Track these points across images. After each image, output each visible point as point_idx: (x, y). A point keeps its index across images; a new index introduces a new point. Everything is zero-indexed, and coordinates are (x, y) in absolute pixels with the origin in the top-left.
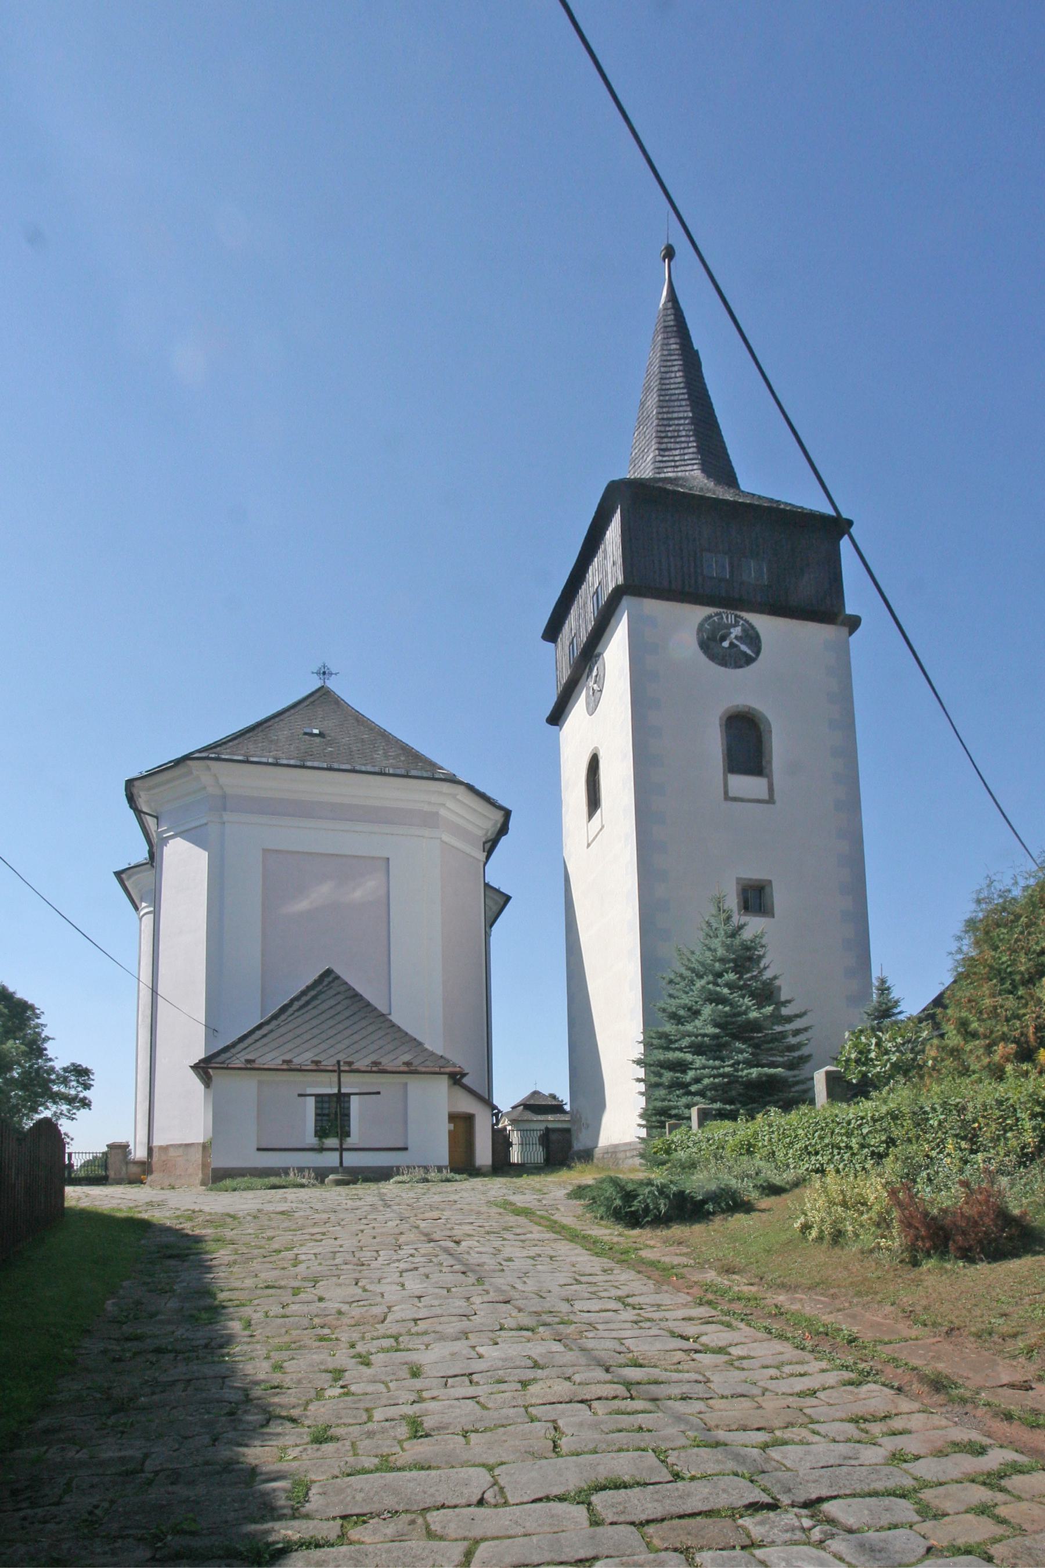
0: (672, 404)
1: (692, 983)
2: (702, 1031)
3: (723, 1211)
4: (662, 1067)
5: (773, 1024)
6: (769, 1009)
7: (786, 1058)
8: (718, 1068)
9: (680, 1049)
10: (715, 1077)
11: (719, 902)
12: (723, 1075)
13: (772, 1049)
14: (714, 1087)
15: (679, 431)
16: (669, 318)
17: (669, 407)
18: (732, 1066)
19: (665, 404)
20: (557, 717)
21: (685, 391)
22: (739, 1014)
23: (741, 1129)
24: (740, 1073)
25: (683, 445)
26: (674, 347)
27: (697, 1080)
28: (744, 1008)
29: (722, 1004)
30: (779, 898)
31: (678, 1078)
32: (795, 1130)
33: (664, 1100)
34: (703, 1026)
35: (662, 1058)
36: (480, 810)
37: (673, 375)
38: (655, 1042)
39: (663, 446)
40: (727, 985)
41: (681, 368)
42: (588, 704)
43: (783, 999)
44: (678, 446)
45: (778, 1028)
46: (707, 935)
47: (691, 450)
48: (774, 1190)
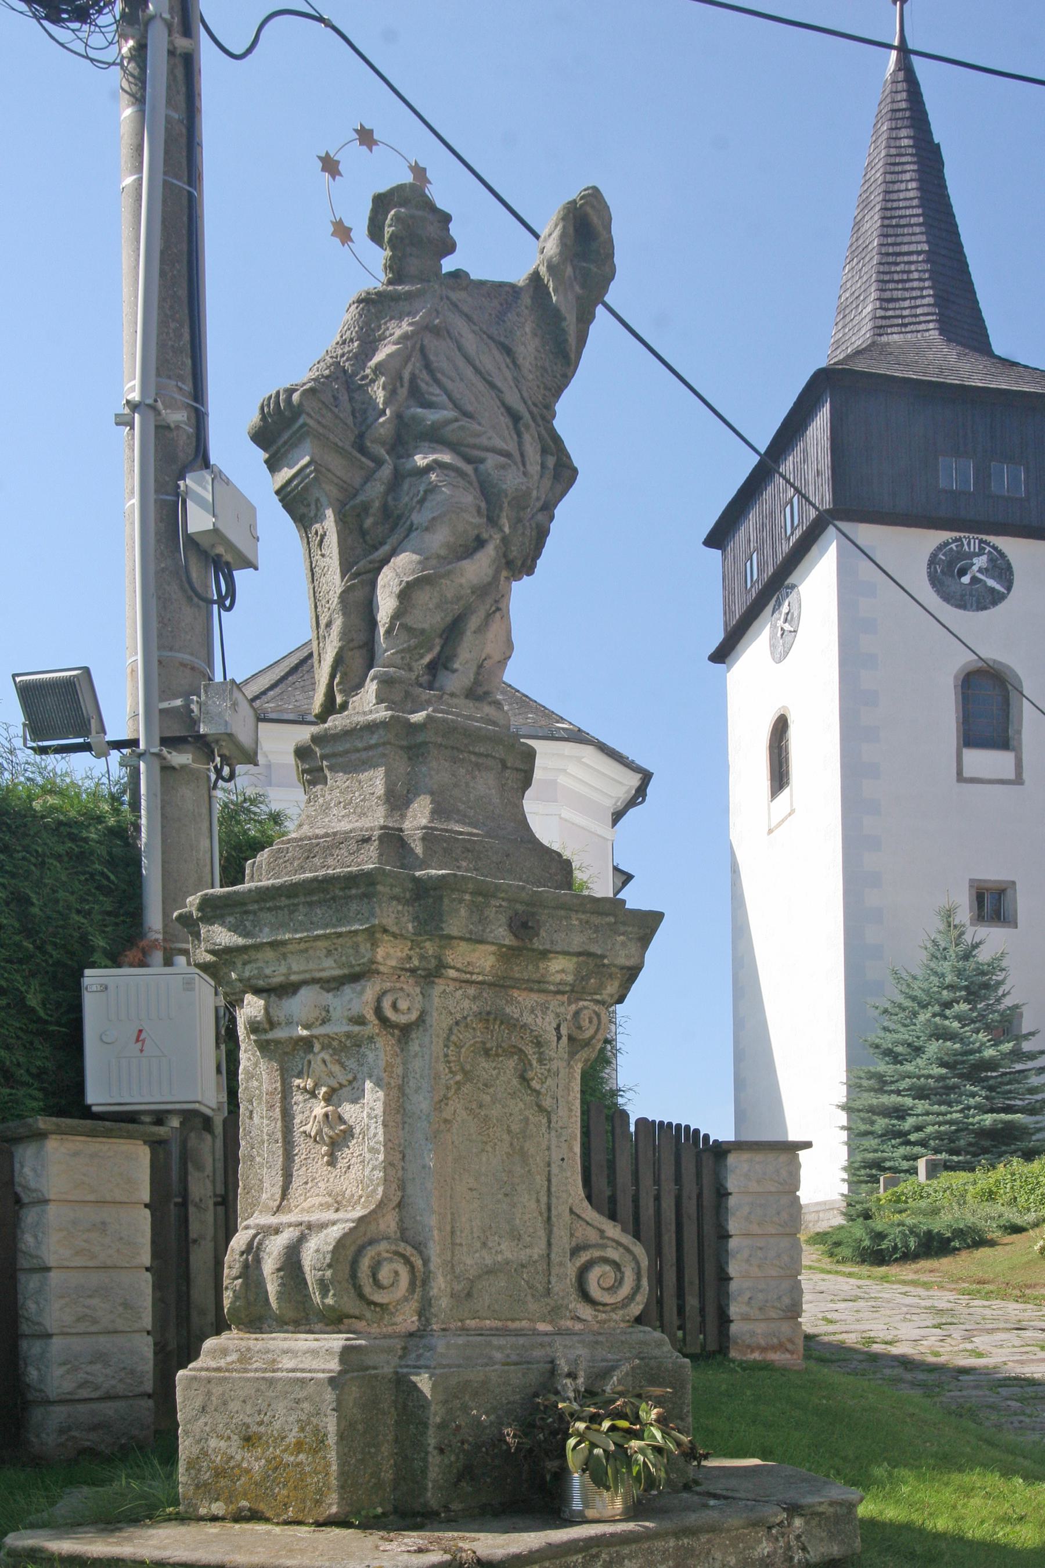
0: (900, 231)
1: (915, 1014)
2: (925, 1072)
3: (969, 1247)
4: (874, 1113)
5: (1012, 1062)
6: (1007, 1047)
7: (1027, 1102)
8: (944, 1114)
9: (898, 1093)
10: (940, 1124)
11: (948, 914)
12: (950, 1123)
13: (1010, 1092)
14: (939, 1136)
15: (909, 272)
16: (899, 97)
17: (897, 235)
18: (961, 1111)
19: (891, 231)
20: (723, 654)
21: (919, 211)
22: (972, 1052)
23: (983, 1179)
24: (971, 1120)
25: (914, 294)
26: (906, 142)
27: (919, 1128)
28: (977, 1045)
29: (950, 1040)
30: (1024, 904)
31: (894, 1126)
32: (1037, 1178)
33: (875, 1151)
34: (927, 1067)
35: (875, 1102)
36: (613, 775)
37: (903, 186)
38: (865, 1083)
39: (887, 295)
40: (958, 1018)
41: (914, 175)
42: (773, 646)
43: (1024, 1031)
44: (907, 295)
45: (1019, 1067)
46: (933, 956)
47: (926, 301)
48: (1016, 1229)
